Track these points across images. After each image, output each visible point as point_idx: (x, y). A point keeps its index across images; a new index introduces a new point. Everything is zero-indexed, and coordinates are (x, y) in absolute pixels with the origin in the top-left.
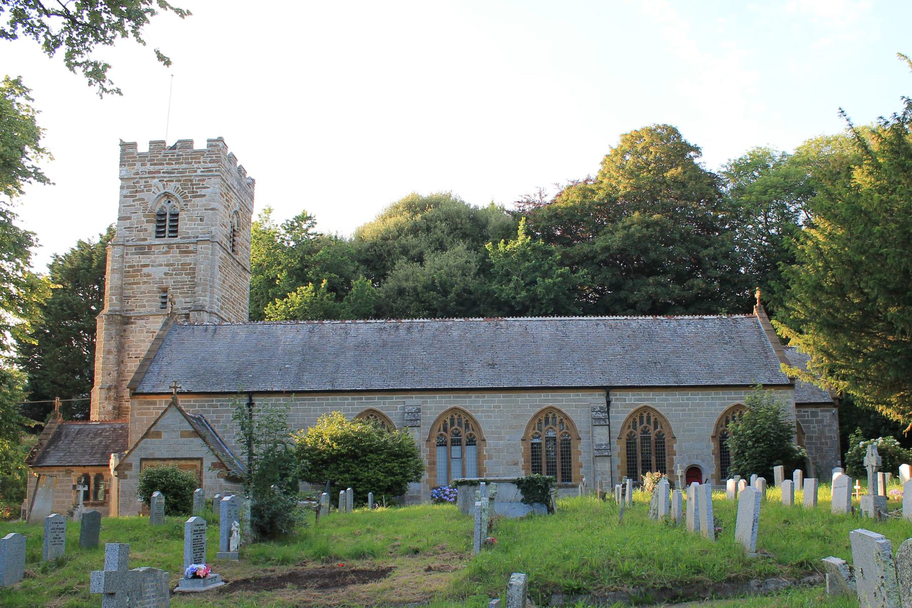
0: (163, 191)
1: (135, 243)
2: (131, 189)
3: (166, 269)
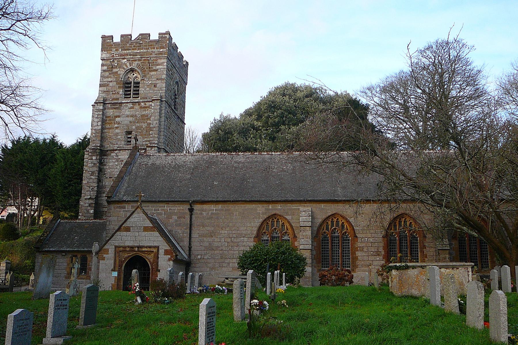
1: (110, 102)
2: (109, 67)
3: (131, 119)
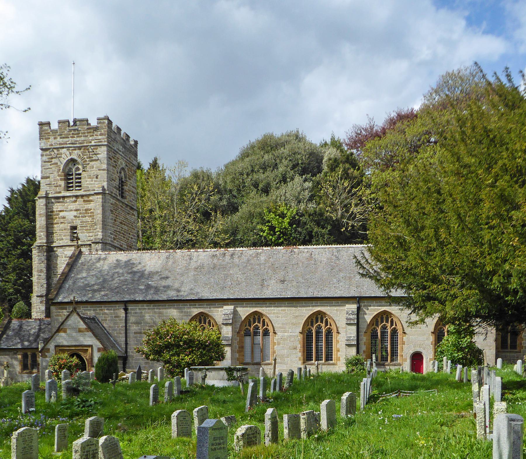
0: (69, 158)
3: (75, 213)
